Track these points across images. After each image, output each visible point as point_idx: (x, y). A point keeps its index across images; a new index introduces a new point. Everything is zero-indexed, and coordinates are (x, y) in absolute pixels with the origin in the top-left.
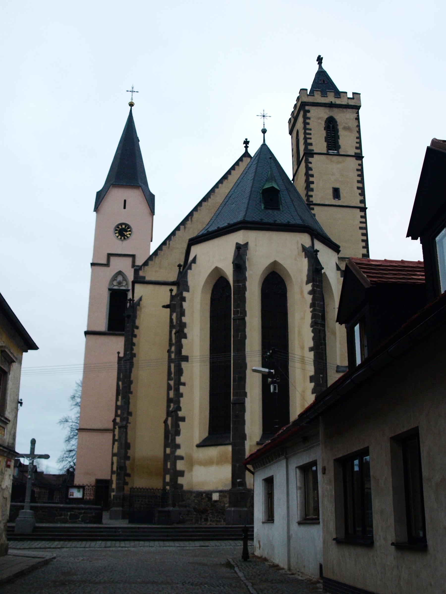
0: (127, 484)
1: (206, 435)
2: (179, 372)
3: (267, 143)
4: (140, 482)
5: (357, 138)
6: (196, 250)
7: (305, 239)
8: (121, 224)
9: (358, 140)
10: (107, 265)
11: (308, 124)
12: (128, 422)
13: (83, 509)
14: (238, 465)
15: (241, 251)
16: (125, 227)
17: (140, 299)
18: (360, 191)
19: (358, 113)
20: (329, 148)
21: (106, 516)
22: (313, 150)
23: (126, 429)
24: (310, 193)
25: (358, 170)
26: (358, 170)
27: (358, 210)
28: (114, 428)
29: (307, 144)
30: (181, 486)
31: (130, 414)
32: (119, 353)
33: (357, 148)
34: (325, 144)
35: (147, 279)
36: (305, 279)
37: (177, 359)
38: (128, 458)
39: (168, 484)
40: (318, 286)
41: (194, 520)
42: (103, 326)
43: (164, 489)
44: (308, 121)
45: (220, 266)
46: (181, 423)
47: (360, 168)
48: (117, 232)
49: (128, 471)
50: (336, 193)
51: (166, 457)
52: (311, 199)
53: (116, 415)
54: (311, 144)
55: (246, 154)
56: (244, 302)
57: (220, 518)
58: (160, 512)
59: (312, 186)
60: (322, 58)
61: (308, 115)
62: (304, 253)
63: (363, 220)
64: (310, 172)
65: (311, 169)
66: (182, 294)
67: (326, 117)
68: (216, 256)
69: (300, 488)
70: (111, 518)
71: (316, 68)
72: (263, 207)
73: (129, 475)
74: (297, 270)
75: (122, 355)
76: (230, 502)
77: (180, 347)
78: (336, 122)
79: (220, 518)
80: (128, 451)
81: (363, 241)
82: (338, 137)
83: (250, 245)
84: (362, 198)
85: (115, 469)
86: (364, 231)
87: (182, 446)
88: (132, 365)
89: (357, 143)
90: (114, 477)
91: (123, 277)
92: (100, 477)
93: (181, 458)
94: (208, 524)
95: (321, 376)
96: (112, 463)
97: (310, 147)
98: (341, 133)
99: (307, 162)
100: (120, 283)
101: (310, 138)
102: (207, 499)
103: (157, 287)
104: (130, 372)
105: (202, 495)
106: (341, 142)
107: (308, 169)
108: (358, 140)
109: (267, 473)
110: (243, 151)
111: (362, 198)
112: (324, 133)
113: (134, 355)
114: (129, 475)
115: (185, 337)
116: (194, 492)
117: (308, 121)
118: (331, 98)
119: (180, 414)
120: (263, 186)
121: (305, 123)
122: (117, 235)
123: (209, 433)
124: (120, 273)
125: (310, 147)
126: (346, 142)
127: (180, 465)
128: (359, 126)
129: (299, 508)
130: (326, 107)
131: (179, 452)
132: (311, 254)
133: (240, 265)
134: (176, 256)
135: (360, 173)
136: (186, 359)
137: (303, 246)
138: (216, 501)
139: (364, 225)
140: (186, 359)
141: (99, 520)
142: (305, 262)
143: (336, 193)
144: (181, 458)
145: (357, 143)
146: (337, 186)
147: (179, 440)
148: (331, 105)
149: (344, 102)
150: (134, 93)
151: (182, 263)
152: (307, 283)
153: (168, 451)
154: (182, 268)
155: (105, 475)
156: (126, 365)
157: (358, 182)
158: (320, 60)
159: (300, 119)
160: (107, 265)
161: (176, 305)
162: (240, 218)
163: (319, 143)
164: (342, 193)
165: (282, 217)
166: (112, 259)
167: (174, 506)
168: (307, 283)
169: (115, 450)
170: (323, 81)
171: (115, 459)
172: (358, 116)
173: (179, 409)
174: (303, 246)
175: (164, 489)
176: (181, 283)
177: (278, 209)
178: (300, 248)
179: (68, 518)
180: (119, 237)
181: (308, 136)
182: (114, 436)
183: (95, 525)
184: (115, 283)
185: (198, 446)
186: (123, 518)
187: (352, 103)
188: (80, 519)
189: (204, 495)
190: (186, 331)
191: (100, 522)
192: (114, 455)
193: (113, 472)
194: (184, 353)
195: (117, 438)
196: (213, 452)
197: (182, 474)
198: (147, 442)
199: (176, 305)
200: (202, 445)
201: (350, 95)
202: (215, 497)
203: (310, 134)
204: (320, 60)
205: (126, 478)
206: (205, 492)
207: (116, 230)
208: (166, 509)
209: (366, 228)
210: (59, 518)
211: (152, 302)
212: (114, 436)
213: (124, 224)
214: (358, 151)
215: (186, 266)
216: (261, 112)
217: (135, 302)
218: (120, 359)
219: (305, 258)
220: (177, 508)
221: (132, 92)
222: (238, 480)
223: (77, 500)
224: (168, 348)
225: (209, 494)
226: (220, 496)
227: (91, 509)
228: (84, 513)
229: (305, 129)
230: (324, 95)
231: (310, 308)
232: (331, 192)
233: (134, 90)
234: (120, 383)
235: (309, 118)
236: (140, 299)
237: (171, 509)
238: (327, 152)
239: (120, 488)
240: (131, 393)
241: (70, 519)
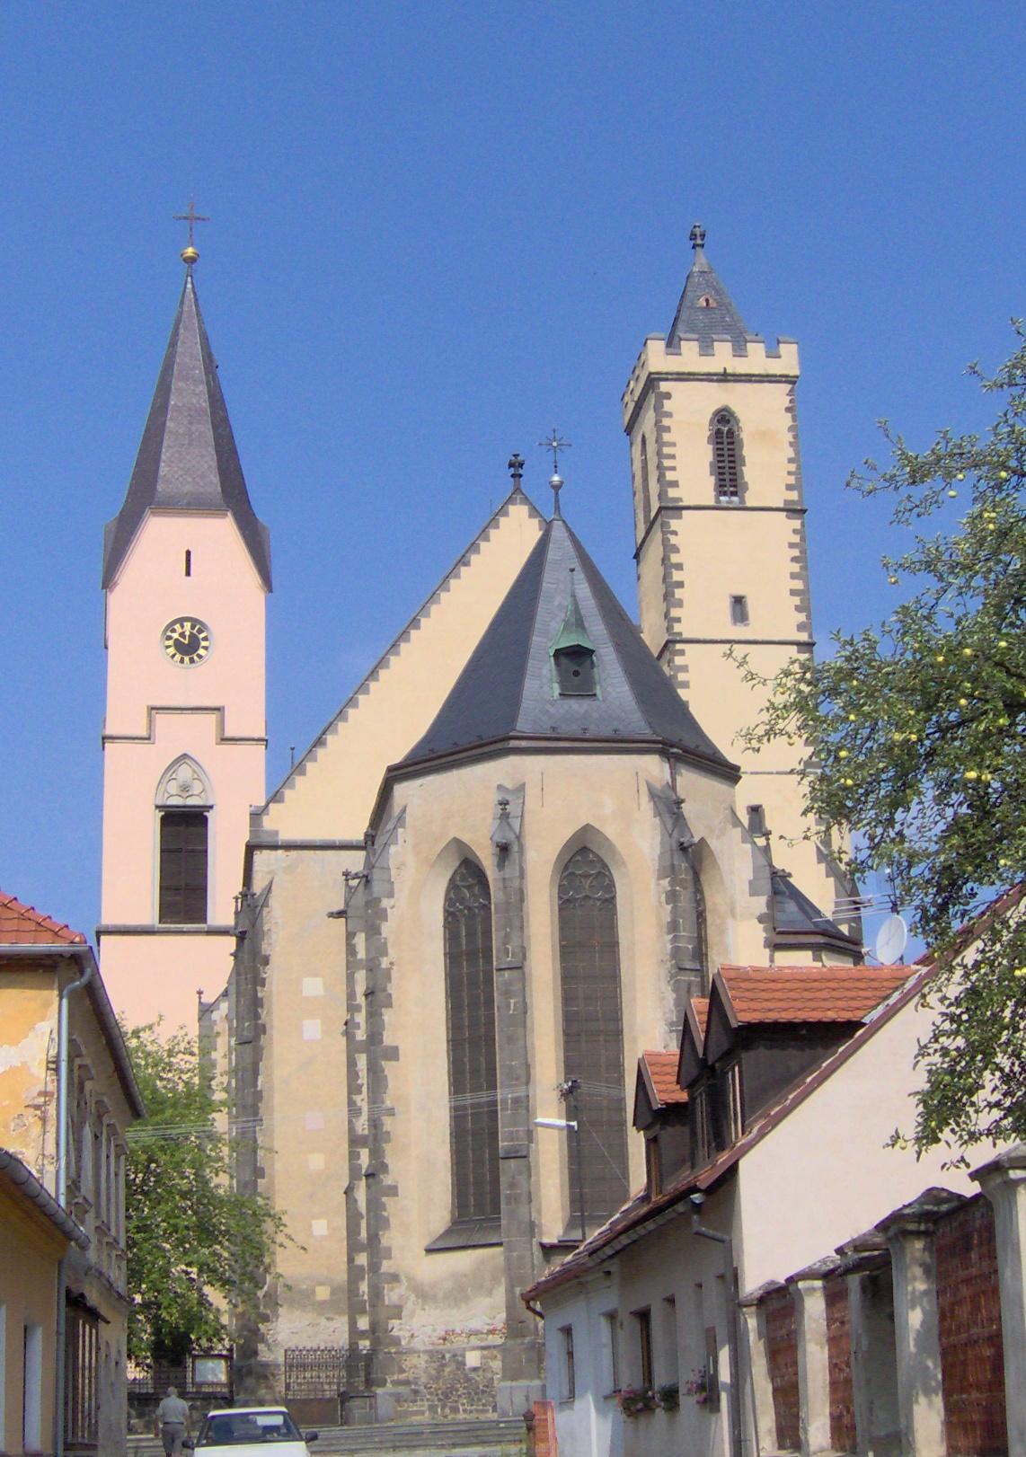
6: (402, 791)
7: (653, 767)
15: (507, 807)
16: (193, 627)
20: (721, 489)
24: (674, 613)
34: (712, 481)
39: (363, 1334)
48: (171, 642)
51: (355, 1273)
52: (677, 628)
59: (678, 593)
64: (674, 558)
65: (676, 550)
74: (638, 849)
94: (461, 1416)
97: (672, 493)
100: (185, 788)
106: (750, 473)
107: (669, 549)
125: (672, 493)
132: (670, 807)
138: (475, 1369)
161: (363, 906)
175: (353, 1347)
180: (178, 657)
184: (173, 788)
196: (463, 1261)
199: (363, 906)
213: (181, 621)
226: (483, 1357)
232: (726, 605)
238: (718, 501)
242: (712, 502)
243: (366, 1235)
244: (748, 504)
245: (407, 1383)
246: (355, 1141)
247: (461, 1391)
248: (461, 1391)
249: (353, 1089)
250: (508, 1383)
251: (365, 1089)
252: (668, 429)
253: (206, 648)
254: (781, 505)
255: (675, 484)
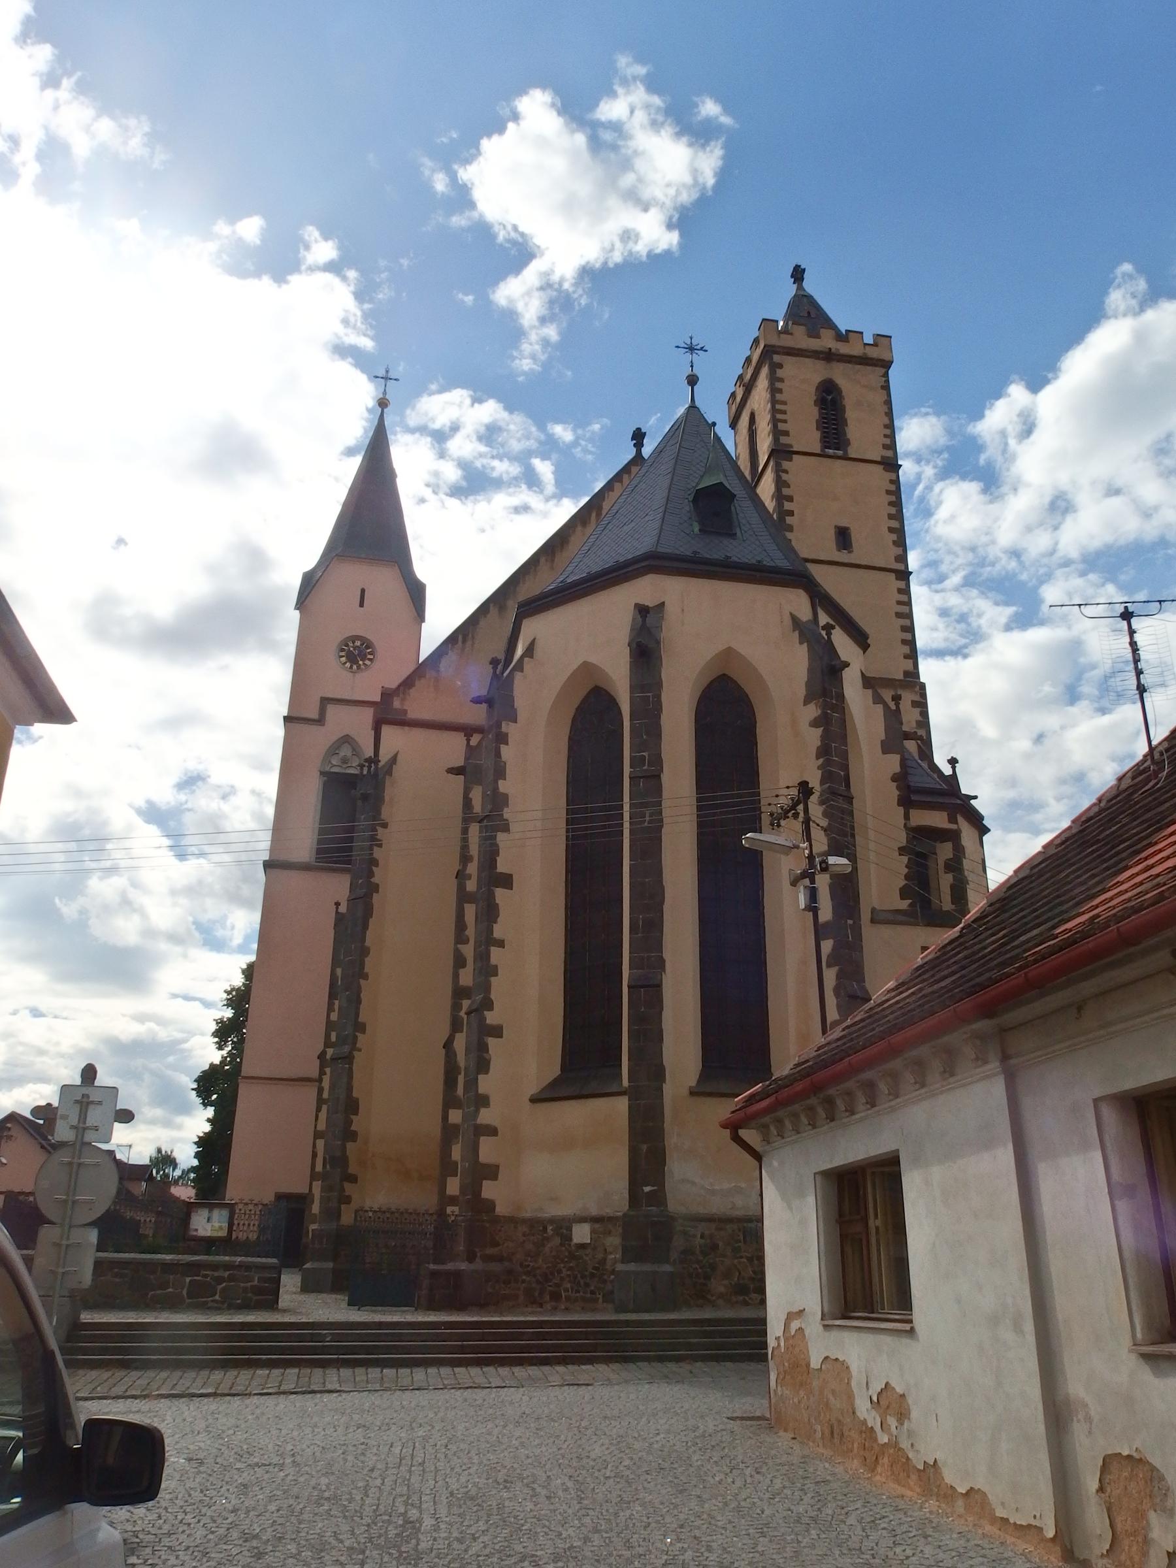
0: (348, 1200)
1: (555, 1071)
2: (490, 913)
3: (697, 403)
4: (378, 1195)
5: (886, 426)
6: (532, 628)
7: (798, 603)
8: (354, 638)
9: (888, 432)
10: (320, 721)
11: (780, 391)
12: (354, 1048)
13: (227, 1266)
14: (645, 1147)
15: (647, 619)
17: (394, 760)
18: (894, 537)
19: (886, 375)
21: (290, 1281)
22: (791, 446)
23: (351, 1063)
25: (888, 492)
26: (888, 492)
27: (893, 576)
28: (322, 1073)
29: (777, 433)
30: (490, 1205)
31: (361, 1028)
32: (337, 904)
33: (885, 447)
34: (817, 435)
35: (412, 715)
36: (802, 692)
37: (482, 887)
38: (352, 1136)
39: (453, 1200)
40: (834, 708)
41: (522, 1298)
42: (304, 847)
43: (441, 1213)
44: (778, 385)
45: (593, 659)
46: (491, 1042)
47: (893, 488)
48: (343, 654)
49: (352, 1170)
50: (843, 537)
51: (449, 1133)
53: (328, 1043)
54: (786, 433)
55: (638, 459)
56: (659, 736)
57: (592, 1293)
58: (434, 1274)
60: (804, 270)
61: (780, 373)
62: (797, 633)
63: (904, 598)
64: (785, 491)
66: (499, 726)
67: (818, 379)
68: (587, 638)
69: (1130, 1191)
70: (306, 1288)
71: (790, 290)
72: (696, 530)
73: (353, 1179)
75: (343, 909)
76: (625, 1250)
77: (491, 854)
78: (839, 391)
79: (592, 1293)
80: (353, 1117)
81: (904, 642)
82: (845, 422)
83: (671, 610)
84: (899, 551)
85: (319, 1168)
86: (907, 622)
87: (493, 1101)
88: (368, 912)
89: (886, 436)
90: (317, 1187)
91: (354, 750)
92: (286, 1188)
93: (492, 1131)
95: (850, 922)
96: (314, 1155)
98: (851, 414)
99: (779, 471)
100: (345, 761)
101: (785, 421)
102: (557, 1241)
103: (433, 735)
104: (365, 926)
105: (545, 1229)
106: (853, 431)
108: (888, 432)
109: (855, 1145)
110: (631, 453)
111: (899, 551)
112: (814, 413)
113: (376, 888)
114: (353, 1179)
115: (506, 828)
116: (524, 1221)
117: (778, 385)
118: (827, 341)
119: (491, 1018)
120: (698, 484)
121: (774, 390)
122: (343, 659)
123: (563, 1068)
124: (346, 740)
126: (861, 434)
127: (487, 1151)
128: (888, 403)
129: (1131, 1281)
130: (818, 358)
131: (485, 1116)
133: (645, 652)
134: (475, 678)
135: (893, 498)
136: (506, 881)
137: (795, 620)
138: (582, 1246)
139: (905, 609)
140: (506, 881)
141: (269, 1297)
142: (802, 652)
143: (843, 537)
144: (492, 1131)
145: (886, 436)
146: (844, 523)
147: (485, 1084)
148: (829, 356)
149: (854, 349)
150: (390, 383)
151: (501, 656)
152: (807, 702)
153: (455, 1116)
154: (500, 667)
155: (298, 1186)
156: (352, 929)
157: (891, 517)
158: (798, 274)
159: (763, 383)
160: (320, 721)
161: (480, 768)
162: (643, 543)
163: (805, 432)
164: (857, 538)
165: (741, 551)
166: (331, 710)
167: (471, 1258)
168: (807, 702)
169: (322, 1126)
170: (806, 312)
171: (320, 1143)
172: (887, 381)
173: (488, 1004)
174: (795, 620)
176: (499, 700)
177: (733, 535)
178: (788, 621)
179: (185, 1292)
180: (348, 665)
181: (779, 416)
182: (320, 1090)
183: (251, 1318)
185: (534, 1100)
186: (336, 1288)
187: (873, 353)
188: (217, 1297)
189: (550, 1228)
190: (507, 813)
191: (271, 1303)
192: (317, 1135)
193: (314, 1176)
194: (502, 867)
195: (325, 1095)
196: (575, 1114)
197: (492, 1172)
198: (398, 1098)
199: (480, 768)
200: (549, 1095)
201: (868, 339)
202: (581, 1234)
203: (784, 412)
204: (798, 274)
205: (347, 1185)
206: (552, 1221)
207: (342, 650)
208: (450, 1266)
209: (910, 616)
210: (159, 1292)
211: (421, 765)
212: (320, 1090)
214: (889, 453)
215: (503, 669)
216: (684, 340)
217: (381, 764)
218: (339, 919)
219: (801, 643)
220: (478, 1265)
221: (386, 378)
222: (647, 1189)
223: (209, 1244)
224: (457, 867)
225: (563, 1227)
226: (593, 1232)
227: (248, 1267)
228: (231, 1278)
229: (774, 401)
230: (814, 334)
231: (818, 758)
232: (831, 534)
233: (391, 375)
234: (339, 971)
235: (781, 380)
236: (394, 760)
237: (463, 1266)
239: (331, 1213)
240: (366, 977)
241: (190, 1296)
242: (818, 451)
243: (460, 1082)
244: (852, 455)
245: (500, 1259)
246: (460, 993)
247: (565, 1272)
248: (565, 1272)
249: (460, 936)
250: (632, 1267)
251: (472, 941)
252: (780, 391)
253: (370, 660)
254: (879, 459)
255: (786, 433)
